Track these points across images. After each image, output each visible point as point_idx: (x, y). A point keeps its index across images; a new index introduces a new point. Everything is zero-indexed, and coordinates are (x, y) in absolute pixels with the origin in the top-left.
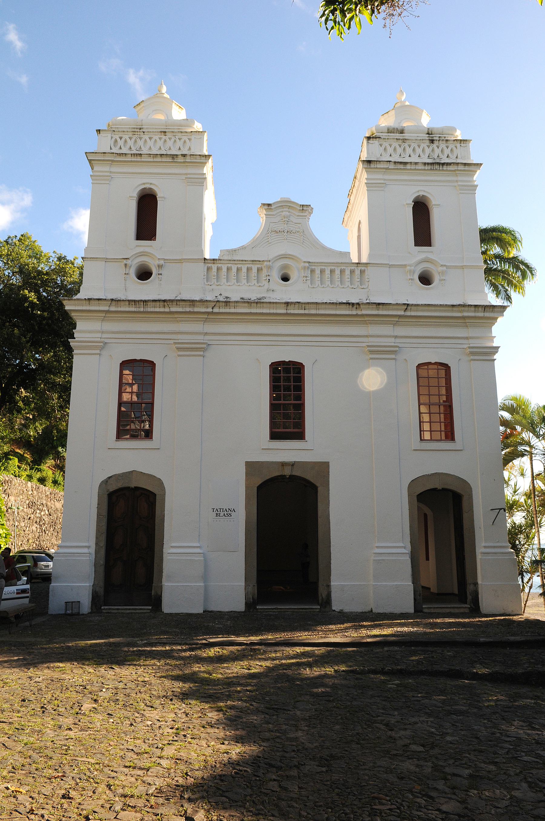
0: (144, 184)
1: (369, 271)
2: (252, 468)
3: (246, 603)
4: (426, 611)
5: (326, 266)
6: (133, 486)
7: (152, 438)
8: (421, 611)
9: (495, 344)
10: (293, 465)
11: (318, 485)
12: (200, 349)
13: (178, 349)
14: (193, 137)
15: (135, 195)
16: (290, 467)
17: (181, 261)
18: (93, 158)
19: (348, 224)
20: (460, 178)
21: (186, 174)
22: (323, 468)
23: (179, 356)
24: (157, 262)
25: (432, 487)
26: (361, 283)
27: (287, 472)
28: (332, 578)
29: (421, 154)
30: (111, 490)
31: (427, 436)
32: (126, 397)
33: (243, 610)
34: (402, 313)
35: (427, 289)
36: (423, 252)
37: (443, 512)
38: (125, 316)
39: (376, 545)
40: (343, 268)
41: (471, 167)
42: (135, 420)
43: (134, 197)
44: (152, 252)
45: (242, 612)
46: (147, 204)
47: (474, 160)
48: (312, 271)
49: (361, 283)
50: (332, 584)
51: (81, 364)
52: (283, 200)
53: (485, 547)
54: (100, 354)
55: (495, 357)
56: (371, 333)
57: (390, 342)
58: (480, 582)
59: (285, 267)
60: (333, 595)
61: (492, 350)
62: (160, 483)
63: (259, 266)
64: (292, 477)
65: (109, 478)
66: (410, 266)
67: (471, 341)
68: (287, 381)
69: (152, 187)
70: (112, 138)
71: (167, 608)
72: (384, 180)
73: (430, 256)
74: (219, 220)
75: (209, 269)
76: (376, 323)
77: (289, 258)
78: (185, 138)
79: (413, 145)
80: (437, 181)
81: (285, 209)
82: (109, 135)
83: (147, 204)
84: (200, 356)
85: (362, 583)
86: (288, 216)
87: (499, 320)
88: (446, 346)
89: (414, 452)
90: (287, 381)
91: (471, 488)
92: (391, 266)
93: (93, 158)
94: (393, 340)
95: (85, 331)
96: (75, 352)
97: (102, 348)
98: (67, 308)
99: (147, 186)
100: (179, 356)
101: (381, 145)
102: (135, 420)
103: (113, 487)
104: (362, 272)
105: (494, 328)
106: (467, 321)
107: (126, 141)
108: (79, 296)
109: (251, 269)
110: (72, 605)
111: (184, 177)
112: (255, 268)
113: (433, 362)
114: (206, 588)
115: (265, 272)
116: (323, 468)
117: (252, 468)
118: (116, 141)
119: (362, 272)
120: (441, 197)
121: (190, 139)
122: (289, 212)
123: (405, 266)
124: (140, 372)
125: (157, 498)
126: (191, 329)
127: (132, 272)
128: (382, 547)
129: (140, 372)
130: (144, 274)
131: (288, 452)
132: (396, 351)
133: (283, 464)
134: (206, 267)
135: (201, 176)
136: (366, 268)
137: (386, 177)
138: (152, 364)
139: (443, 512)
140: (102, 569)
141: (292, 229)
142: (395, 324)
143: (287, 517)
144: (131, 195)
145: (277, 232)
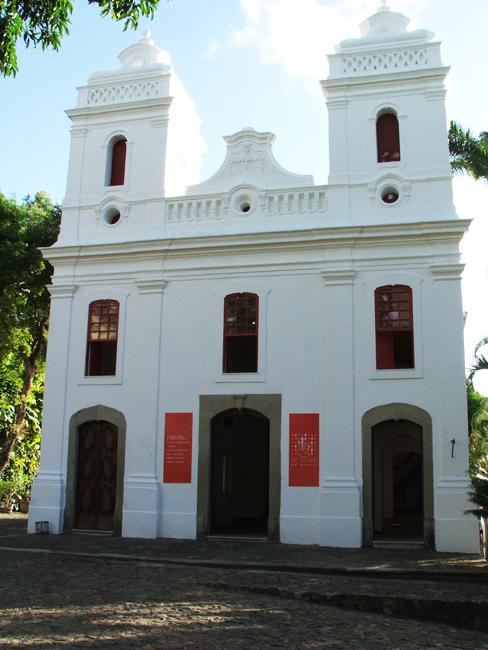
1: (328, 194)
3: (197, 532)
4: (376, 546)
6: (98, 419)
8: (372, 547)
9: (461, 262)
10: (244, 397)
13: (325, 278)
14: (427, 49)
15: (375, 117)
16: (241, 401)
17: (144, 202)
18: (73, 115)
19: (310, 148)
20: (427, 85)
21: (425, 88)
23: (327, 285)
24: (125, 205)
25: (388, 418)
26: (320, 206)
27: (239, 405)
28: (281, 510)
30: (80, 423)
32: (95, 336)
33: (282, 541)
34: (357, 235)
36: (389, 167)
37: (397, 449)
39: (442, 478)
40: (307, 194)
41: (440, 73)
42: (101, 359)
45: (193, 541)
47: (445, 65)
48: (271, 199)
49: (320, 206)
50: (281, 516)
51: (57, 306)
53: (443, 481)
54: (352, 284)
57: (347, 266)
58: (436, 517)
59: (243, 197)
60: (282, 528)
64: (243, 409)
66: (371, 184)
68: (242, 313)
69: (390, 106)
71: (124, 535)
73: (393, 171)
74: (185, 160)
75: (171, 206)
76: (241, 253)
79: (410, 52)
82: (87, 90)
85: (311, 517)
86: (249, 146)
87: (465, 235)
90: (242, 313)
91: (430, 419)
92: (351, 186)
93: (73, 115)
94: (350, 264)
95: (61, 276)
96: (52, 296)
97: (164, 287)
99: (386, 106)
100: (327, 285)
101: (344, 61)
102: (101, 359)
105: (461, 243)
107: (360, 62)
110: (43, 525)
112: (204, 202)
114: (160, 517)
115: (223, 205)
118: (93, 95)
119: (321, 195)
123: (367, 184)
124: (105, 312)
126: (151, 269)
128: (447, 481)
129: (105, 312)
130: (390, 196)
131: (241, 385)
133: (235, 397)
137: (348, 94)
138: (407, 290)
139: (397, 449)
140: (72, 496)
143: (240, 451)
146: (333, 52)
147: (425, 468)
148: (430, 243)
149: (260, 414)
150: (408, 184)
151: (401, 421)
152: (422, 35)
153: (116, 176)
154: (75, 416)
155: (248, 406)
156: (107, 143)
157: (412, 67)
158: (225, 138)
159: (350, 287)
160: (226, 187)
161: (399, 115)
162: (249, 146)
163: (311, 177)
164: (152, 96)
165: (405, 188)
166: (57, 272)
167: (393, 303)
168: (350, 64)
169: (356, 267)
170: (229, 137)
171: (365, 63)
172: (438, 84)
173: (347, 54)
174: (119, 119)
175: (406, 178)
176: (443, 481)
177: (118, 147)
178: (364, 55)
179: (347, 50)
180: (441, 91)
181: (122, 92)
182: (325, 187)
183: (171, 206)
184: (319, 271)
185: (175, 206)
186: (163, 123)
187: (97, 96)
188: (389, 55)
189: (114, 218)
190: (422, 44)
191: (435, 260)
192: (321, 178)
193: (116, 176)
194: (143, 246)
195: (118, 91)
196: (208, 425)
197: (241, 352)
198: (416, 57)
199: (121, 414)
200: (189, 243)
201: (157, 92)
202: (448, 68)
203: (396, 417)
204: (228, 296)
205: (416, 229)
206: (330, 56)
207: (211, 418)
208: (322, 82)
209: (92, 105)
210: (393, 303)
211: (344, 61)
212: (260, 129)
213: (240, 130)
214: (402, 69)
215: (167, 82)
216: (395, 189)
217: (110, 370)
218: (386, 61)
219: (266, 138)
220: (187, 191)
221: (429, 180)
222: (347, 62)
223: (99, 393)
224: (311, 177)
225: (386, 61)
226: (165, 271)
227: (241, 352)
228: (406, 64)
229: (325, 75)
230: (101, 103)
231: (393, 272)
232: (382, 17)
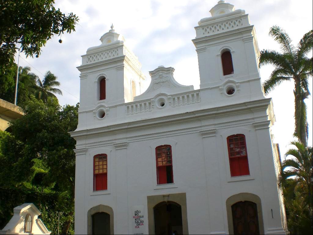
0: (100, 75)
1: (201, 94)
2: (150, 199)
5: (175, 96)
6: (100, 211)
7: (107, 189)
10: (168, 196)
11: (181, 205)
12: (124, 146)
14: (242, 18)
17: (116, 106)
20: (244, 35)
21: (242, 37)
22: (183, 196)
23: (256, 130)
27: (166, 200)
29: (219, 29)
30: (92, 214)
31: (287, 169)
32: (97, 172)
34: (126, 127)
35: (231, 96)
36: (229, 77)
38: (211, 116)
39: (269, 229)
40: (189, 94)
42: (100, 181)
43: (219, 55)
44: (105, 103)
46: (226, 57)
52: (159, 67)
53: (269, 231)
54: (85, 154)
55: (269, 126)
56: (203, 125)
57: (212, 128)
61: (267, 123)
62: (111, 209)
63: (149, 101)
64: (168, 202)
65: (91, 209)
66: (221, 86)
67: (255, 120)
70: (87, 57)
72: (205, 46)
73: (231, 79)
75: (128, 107)
77: (163, 95)
78: (116, 50)
80: (229, 40)
81: (160, 72)
82: (86, 57)
83: (226, 57)
84: (84, 154)
86: (162, 75)
88: (242, 125)
89: (229, 183)
95: (79, 145)
98: (71, 136)
99: (225, 48)
100: (117, 150)
101: (203, 29)
102: (100, 181)
103: (93, 212)
104: (198, 95)
106: (251, 110)
108: (76, 130)
109: (194, 95)
111: (115, 68)
113: (163, 145)
115: (152, 104)
116: (183, 196)
117: (150, 199)
118: (89, 59)
120: (234, 47)
121: (117, 50)
122: (162, 72)
123: (219, 87)
124: (101, 158)
125: (258, 206)
126: (120, 138)
127: (225, 92)
129: (101, 158)
130: (230, 92)
131: (166, 190)
132: (126, 145)
133: (164, 196)
134: (126, 107)
135: (249, 37)
136: (199, 92)
141: (164, 80)
142: (214, 118)
144: (95, 81)
145: (157, 83)
146: (198, 25)
147: (260, 225)
148: (252, 112)
149: (176, 203)
150: (108, 108)
151: (245, 202)
152: (239, 12)
153: (102, 96)
154: (90, 211)
155: (170, 200)
156: (97, 80)
157: (236, 28)
158: (149, 72)
159: (125, 150)
160: (152, 96)
161: (231, 51)
162: (162, 75)
163: (192, 86)
164: (116, 56)
165: (107, 111)
166: (78, 143)
167: (237, 143)
168: (206, 30)
169: (216, 127)
170: (152, 71)
171: (213, 29)
172: (250, 34)
173: (203, 25)
174: (96, 70)
175: (237, 82)
176: (269, 231)
177: (102, 82)
178: (212, 25)
179: (203, 24)
180: (250, 38)
181: (102, 56)
182: (199, 91)
183: (128, 107)
184: (199, 131)
185: (140, 103)
186: (122, 68)
187: (91, 59)
188: (210, 27)
189: (102, 115)
190: (241, 16)
191: (202, 128)
192: (197, 87)
193: (102, 96)
194: (166, 119)
195: (104, 54)
196: (152, 211)
197: (165, 174)
198: (237, 23)
199: (111, 208)
200: (137, 124)
201: (118, 54)
202: (253, 26)
203: (243, 200)
204: (228, 137)
205: (258, 104)
206: (196, 28)
207: (153, 207)
208: (193, 40)
209: (89, 63)
210: (237, 143)
211: (203, 29)
212: (167, 66)
213: (157, 67)
214: (231, 29)
215: (122, 48)
216: (234, 89)
217: (170, 180)
218: (223, 26)
219: (170, 70)
220: (134, 99)
221: (249, 81)
222: (204, 29)
223: (101, 199)
224: (192, 86)
225: (223, 26)
226: (86, 144)
227: (165, 174)
228: (228, 28)
229: (194, 37)
230: (93, 62)
231: (238, 128)
232: (221, 5)
